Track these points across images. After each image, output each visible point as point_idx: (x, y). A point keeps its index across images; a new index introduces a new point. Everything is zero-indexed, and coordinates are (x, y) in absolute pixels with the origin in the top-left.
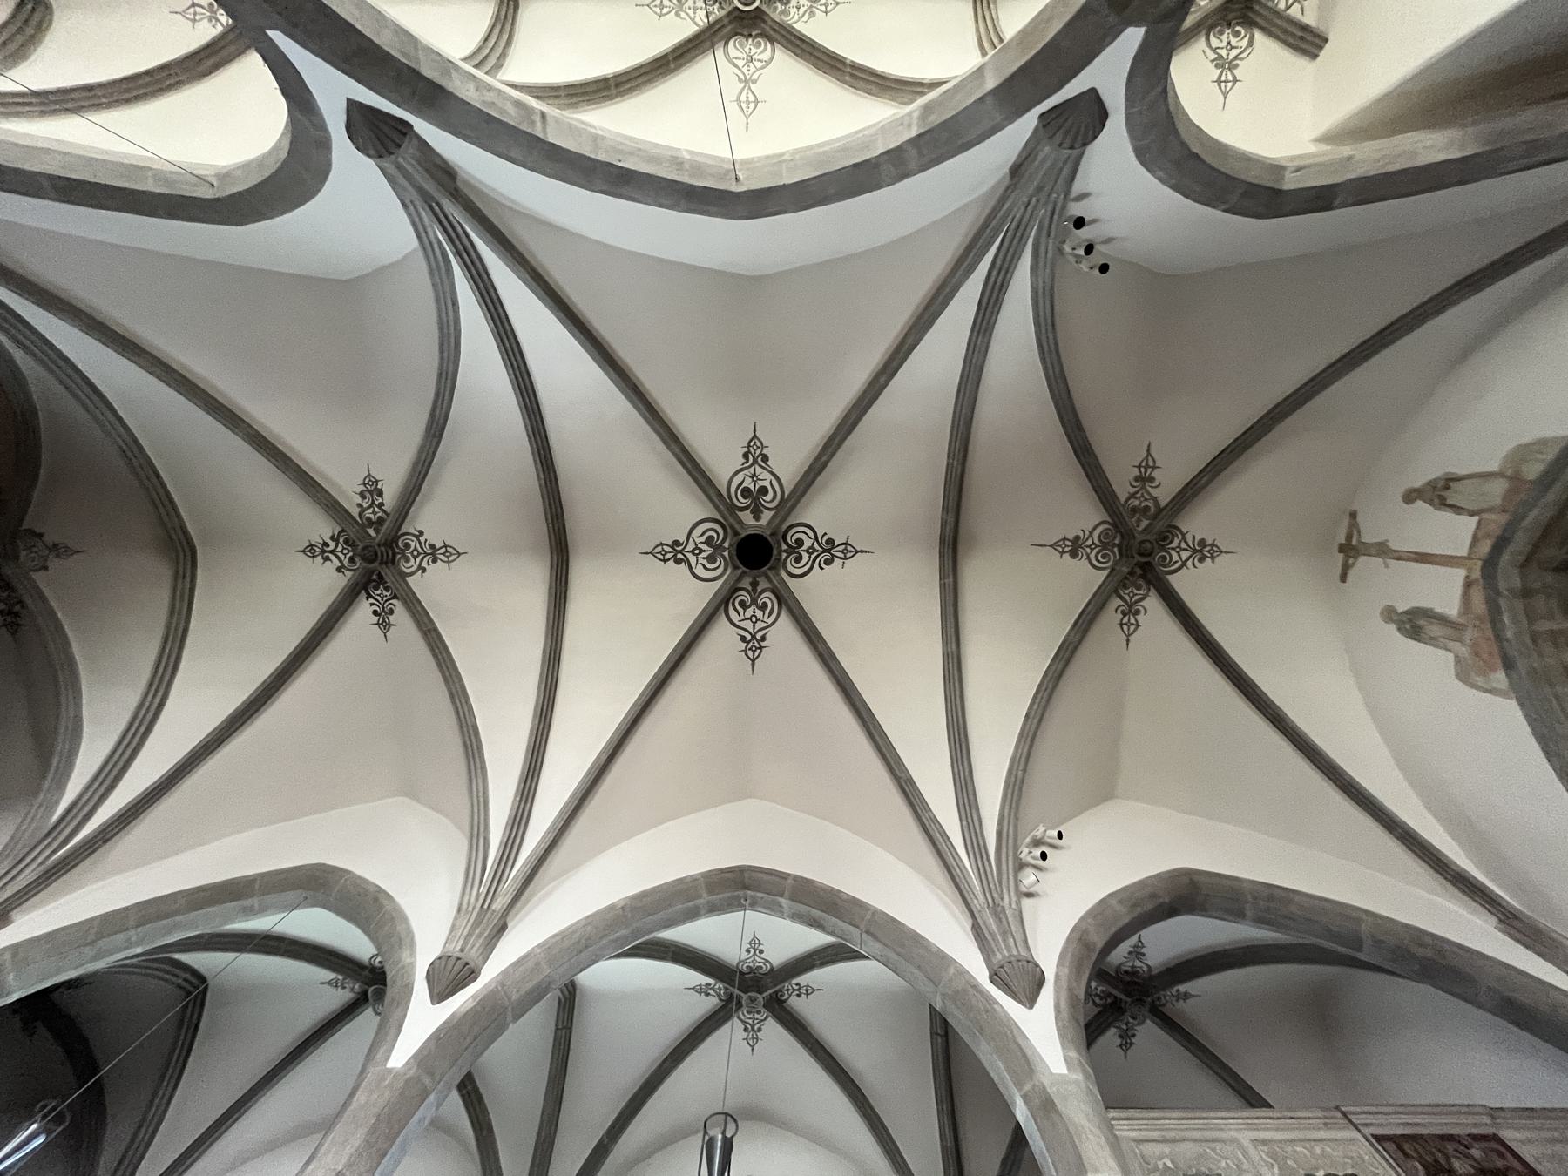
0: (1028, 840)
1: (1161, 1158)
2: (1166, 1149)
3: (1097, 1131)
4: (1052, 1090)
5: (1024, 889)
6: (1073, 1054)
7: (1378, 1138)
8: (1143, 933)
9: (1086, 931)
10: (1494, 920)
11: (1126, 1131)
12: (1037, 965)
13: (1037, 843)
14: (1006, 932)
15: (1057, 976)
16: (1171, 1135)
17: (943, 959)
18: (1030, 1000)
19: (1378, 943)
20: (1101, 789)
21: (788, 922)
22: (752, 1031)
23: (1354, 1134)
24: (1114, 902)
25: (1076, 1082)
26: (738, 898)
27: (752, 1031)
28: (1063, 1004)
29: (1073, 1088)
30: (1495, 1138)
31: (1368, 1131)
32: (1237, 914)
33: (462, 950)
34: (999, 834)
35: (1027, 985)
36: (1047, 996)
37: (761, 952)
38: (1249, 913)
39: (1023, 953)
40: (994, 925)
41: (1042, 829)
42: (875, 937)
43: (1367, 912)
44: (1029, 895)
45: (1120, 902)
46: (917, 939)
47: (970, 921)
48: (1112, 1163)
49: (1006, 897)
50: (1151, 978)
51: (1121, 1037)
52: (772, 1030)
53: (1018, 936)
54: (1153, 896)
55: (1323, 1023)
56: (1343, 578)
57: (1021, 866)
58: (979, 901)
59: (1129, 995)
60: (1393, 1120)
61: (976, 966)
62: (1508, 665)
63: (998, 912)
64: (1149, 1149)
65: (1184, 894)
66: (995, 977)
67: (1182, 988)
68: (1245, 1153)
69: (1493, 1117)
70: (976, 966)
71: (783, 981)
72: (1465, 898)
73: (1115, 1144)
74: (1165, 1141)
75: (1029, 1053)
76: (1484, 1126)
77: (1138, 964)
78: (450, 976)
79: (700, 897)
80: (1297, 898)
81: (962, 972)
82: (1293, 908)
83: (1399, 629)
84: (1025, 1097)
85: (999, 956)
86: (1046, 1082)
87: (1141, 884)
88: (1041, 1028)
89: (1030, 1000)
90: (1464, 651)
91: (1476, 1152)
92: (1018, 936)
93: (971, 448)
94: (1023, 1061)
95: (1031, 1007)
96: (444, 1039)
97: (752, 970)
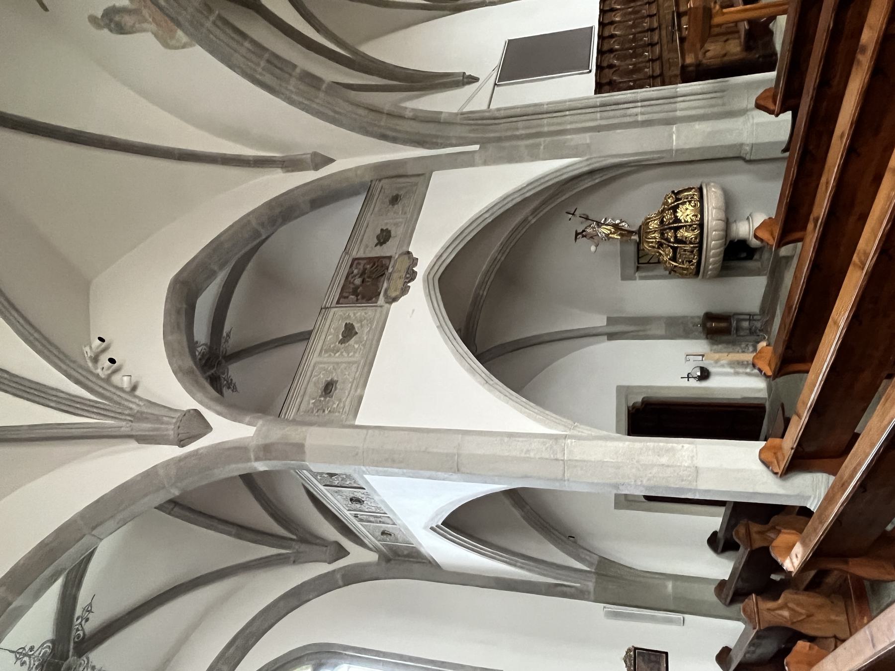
0: (90, 364)
2: (306, 398)
3: (288, 428)
4: (262, 442)
5: (128, 390)
6: (247, 419)
7: (338, 303)
8: (686, 616)
9: (180, 367)
10: (279, 170)
11: (291, 414)
12: (189, 411)
13: (95, 360)
14: (157, 419)
15: (201, 403)
16: (302, 392)
17: (150, 475)
18: (207, 428)
19: (262, 225)
20: (79, 287)
21: (36, 605)
23: (334, 310)
24: (170, 338)
25: (263, 425)
28: (219, 408)
29: (264, 429)
30: (354, 260)
31: (334, 304)
32: (212, 275)
34: (77, 382)
35: (194, 425)
36: (210, 416)
37: (32, 649)
38: (216, 268)
39: (177, 415)
40: (143, 423)
41: (87, 349)
43: (248, 215)
44: (134, 388)
45: (172, 333)
46: (123, 490)
48: (304, 429)
49: (131, 405)
50: (210, 348)
51: (229, 388)
53: (163, 412)
54: (178, 312)
55: (275, 280)
56: (46, 9)
57: (108, 380)
58: (125, 427)
59: (212, 367)
60: (333, 293)
62: (179, 25)
63: (139, 417)
64: (303, 408)
65: (184, 292)
66: (181, 443)
67: (225, 334)
68: (321, 363)
69: (347, 253)
72: (266, 170)
73: (295, 422)
75: (237, 445)
76: (348, 261)
77: (199, 349)
80: (222, 238)
81: (166, 464)
82: (226, 246)
83: (111, 31)
85: (171, 433)
86: (254, 443)
87: (167, 313)
88: (226, 430)
89: (207, 428)
90: (153, 27)
91: (356, 271)
92: (163, 412)
93: (542, 346)
94: (236, 451)
95: (211, 429)
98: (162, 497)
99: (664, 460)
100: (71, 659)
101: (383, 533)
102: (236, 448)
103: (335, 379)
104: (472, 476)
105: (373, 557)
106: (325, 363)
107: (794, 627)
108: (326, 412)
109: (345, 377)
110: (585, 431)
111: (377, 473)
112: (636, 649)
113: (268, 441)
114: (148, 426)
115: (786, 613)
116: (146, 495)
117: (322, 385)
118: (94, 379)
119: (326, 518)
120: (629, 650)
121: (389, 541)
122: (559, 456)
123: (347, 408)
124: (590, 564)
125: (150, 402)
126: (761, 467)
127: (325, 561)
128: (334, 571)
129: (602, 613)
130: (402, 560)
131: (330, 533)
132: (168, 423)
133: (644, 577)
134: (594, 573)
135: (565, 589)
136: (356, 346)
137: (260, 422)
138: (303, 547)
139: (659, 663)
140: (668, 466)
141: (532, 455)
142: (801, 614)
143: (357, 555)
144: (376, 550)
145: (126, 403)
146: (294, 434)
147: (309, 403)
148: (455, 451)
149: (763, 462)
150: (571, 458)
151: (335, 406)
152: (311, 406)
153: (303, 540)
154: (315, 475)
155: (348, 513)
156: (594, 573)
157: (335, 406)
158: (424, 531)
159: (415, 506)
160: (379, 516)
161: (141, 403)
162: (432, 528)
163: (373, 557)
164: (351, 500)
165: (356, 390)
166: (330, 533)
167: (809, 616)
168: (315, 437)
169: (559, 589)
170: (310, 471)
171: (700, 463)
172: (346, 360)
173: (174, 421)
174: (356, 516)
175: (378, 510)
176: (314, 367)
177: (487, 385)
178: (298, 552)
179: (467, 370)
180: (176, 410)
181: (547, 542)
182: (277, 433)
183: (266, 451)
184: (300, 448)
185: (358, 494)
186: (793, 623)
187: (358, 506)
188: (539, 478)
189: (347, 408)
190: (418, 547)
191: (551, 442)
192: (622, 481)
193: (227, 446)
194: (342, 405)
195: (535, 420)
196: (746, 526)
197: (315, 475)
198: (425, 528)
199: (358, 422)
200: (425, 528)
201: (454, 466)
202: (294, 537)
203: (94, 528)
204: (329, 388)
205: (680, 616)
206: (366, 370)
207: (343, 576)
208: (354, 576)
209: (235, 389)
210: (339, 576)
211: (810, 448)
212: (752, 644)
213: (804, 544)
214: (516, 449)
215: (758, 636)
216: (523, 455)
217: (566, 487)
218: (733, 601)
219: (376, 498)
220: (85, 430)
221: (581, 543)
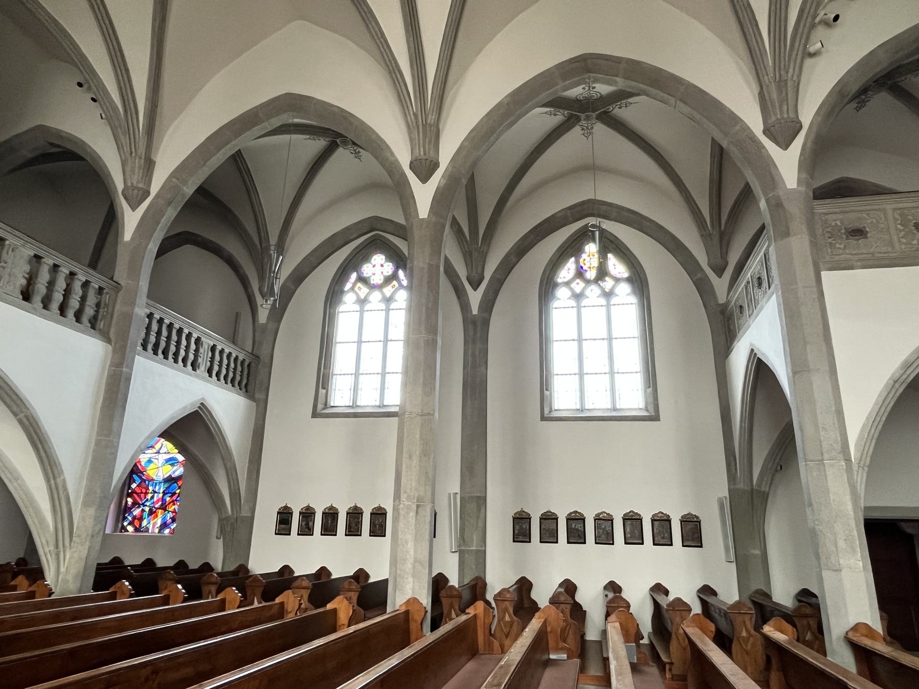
1: (835, 220)
2: (841, 216)
8: (734, 564)
14: (784, 100)
18: (785, 145)
22: (588, 132)
26: (585, 79)
27: (588, 132)
33: (425, 154)
34: (802, 11)
40: (777, 93)
42: (685, 103)
44: (811, 55)
46: (716, 105)
47: (759, 89)
52: (600, 129)
61: (754, 121)
63: (781, 84)
66: (766, 132)
68: (885, 215)
70: (754, 121)
71: (609, 105)
74: (842, 212)
78: (424, 169)
79: (556, 84)
81: (746, 128)
84: (767, 201)
86: (781, 193)
88: (788, 163)
89: (785, 145)
96: (441, 200)
97: (586, 98)
98: (719, 137)
99: (841, 544)
100: (594, 115)
101: (741, 307)
102: (773, 179)
103: (869, 235)
104: (793, 383)
105: (722, 299)
106: (886, 218)
107: (735, 639)
108: (830, 240)
109: (874, 244)
110: (860, 478)
111: (779, 305)
112: (700, 522)
113: (786, 204)
114: (775, 95)
115: (744, 634)
116: (715, 124)
117: (857, 225)
118: (803, 41)
119: (746, 249)
120: (697, 517)
121: (736, 312)
122: (826, 456)
123: (837, 258)
124: (759, 485)
125: (799, 84)
126: (852, 623)
127: (709, 260)
128: (702, 270)
129: (720, 495)
130: (725, 325)
131: (734, 258)
132: (781, 111)
133: (759, 530)
134: (752, 489)
135: (733, 464)
136: (915, 242)
137: (803, 189)
138: (716, 239)
139: (693, 540)
140: (836, 547)
141: (822, 433)
142: (747, 645)
143: (720, 285)
144: (728, 302)
145: (792, 66)
146: (798, 225)
147: (835, 220)
148: (812, 367)
149: (857, 624)
150: (827, 466)
151: (838, 245)
152: (833, 224)
153: (722, 235)
154: (767, 249)
155: (749, 275)
156: (752, 489)
157: (838, 245)
158: (748, 346)
159: (764, 334)
160: (754, 303)
161: (795, 78)
162: (752, 350)
163: (722, 299)
164: (759, 278)
165: (858, 260)
166: (734, 258)
167: (747, 653)
168: (799, 243)
169: (732, 458)
170: (769, 246)
171: (845, 574)
172: (895, 238)
173: (785, 116)
174: (748, 282)
175: (757, 302)
176: (879, 210)
177: (892, 382)
178: (710, 235)
179: (906, 361)
180: (796, 111)
181: (769, 447)
182: (795, 209)
183: (777, 206)
184: (786, 234)
185: (765, 284)
186: (738, 639)
187: (756, 284)
188: (803, 441)
189: (837, 258)
190: (737, 339)
191: (838, 447)
192: (815, 507)
193: (773, 170)
194: (841, 251)
195: (862, 431)
196: (808, 611)
197: (767, 249)
198: (751, 344)
199: (824, 274)
200: (751, 344)
201: (798, 368)
202: (723, 228)
203: (681, 100)
204: (858, 233)
205: (733, 559)
206: (887, 262)
207: (701, 279)
208: (703, 287)
209: (858, 109)
210: (699, 275)
211: (880, 667)
212: (720, 609)
213: (790, 642)
214: (826, 419)
215: (726, 614)
216: (820, 426)
217: (802, 464)
218: (754, 603)
219: (765, 299)
220: (758, 53)
221: (778, 476)
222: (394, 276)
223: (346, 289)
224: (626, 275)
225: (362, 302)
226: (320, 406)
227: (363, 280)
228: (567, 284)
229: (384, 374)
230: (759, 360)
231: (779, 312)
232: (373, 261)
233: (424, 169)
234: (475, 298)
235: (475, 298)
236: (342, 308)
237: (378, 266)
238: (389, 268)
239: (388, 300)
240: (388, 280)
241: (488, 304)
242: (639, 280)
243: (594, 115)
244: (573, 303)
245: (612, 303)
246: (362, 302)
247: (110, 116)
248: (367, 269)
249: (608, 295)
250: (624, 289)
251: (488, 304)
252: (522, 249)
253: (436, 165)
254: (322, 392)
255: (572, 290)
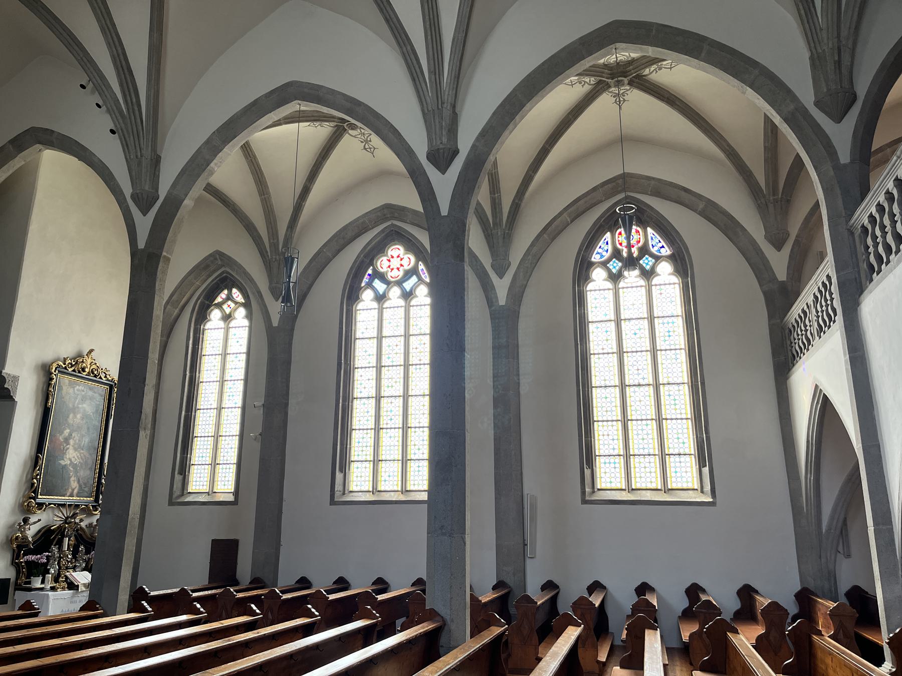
22: (619, 100)
27: (619, 100)
78: (442, 158)
89: (838, 118)
100: (626, 80)
130: (784, 355)
162: (817, 386)
222: (414, 271)
223: (363, 284)
224: (669, 253)
225: (381, 298)
226: (337, 494)
227: (382, 277)
228: (604, 264)
229: (407, 336)
230: (825, 396)
231: (843, 344)
232: (390, 253)
233: (442, 158)
234: (502, 287)
235: (502, 287)
236: (360, 306)
237: (396, 259)
238: (409, 260)
239: (408, 296)
240: (408, 274)
241: (517, 294)
242: (681, 262)
243: (626, 80)
244: (609, 285)
245: (653, 283)
246: (381, 298)
247: (107, 103)
248: (382, 264)
249: (648, 275)
250: (665, 269)
251: (517, 294)
252: (552, 232)
253: (456, 152)
254: (339, 476)
255: (609, 271)
